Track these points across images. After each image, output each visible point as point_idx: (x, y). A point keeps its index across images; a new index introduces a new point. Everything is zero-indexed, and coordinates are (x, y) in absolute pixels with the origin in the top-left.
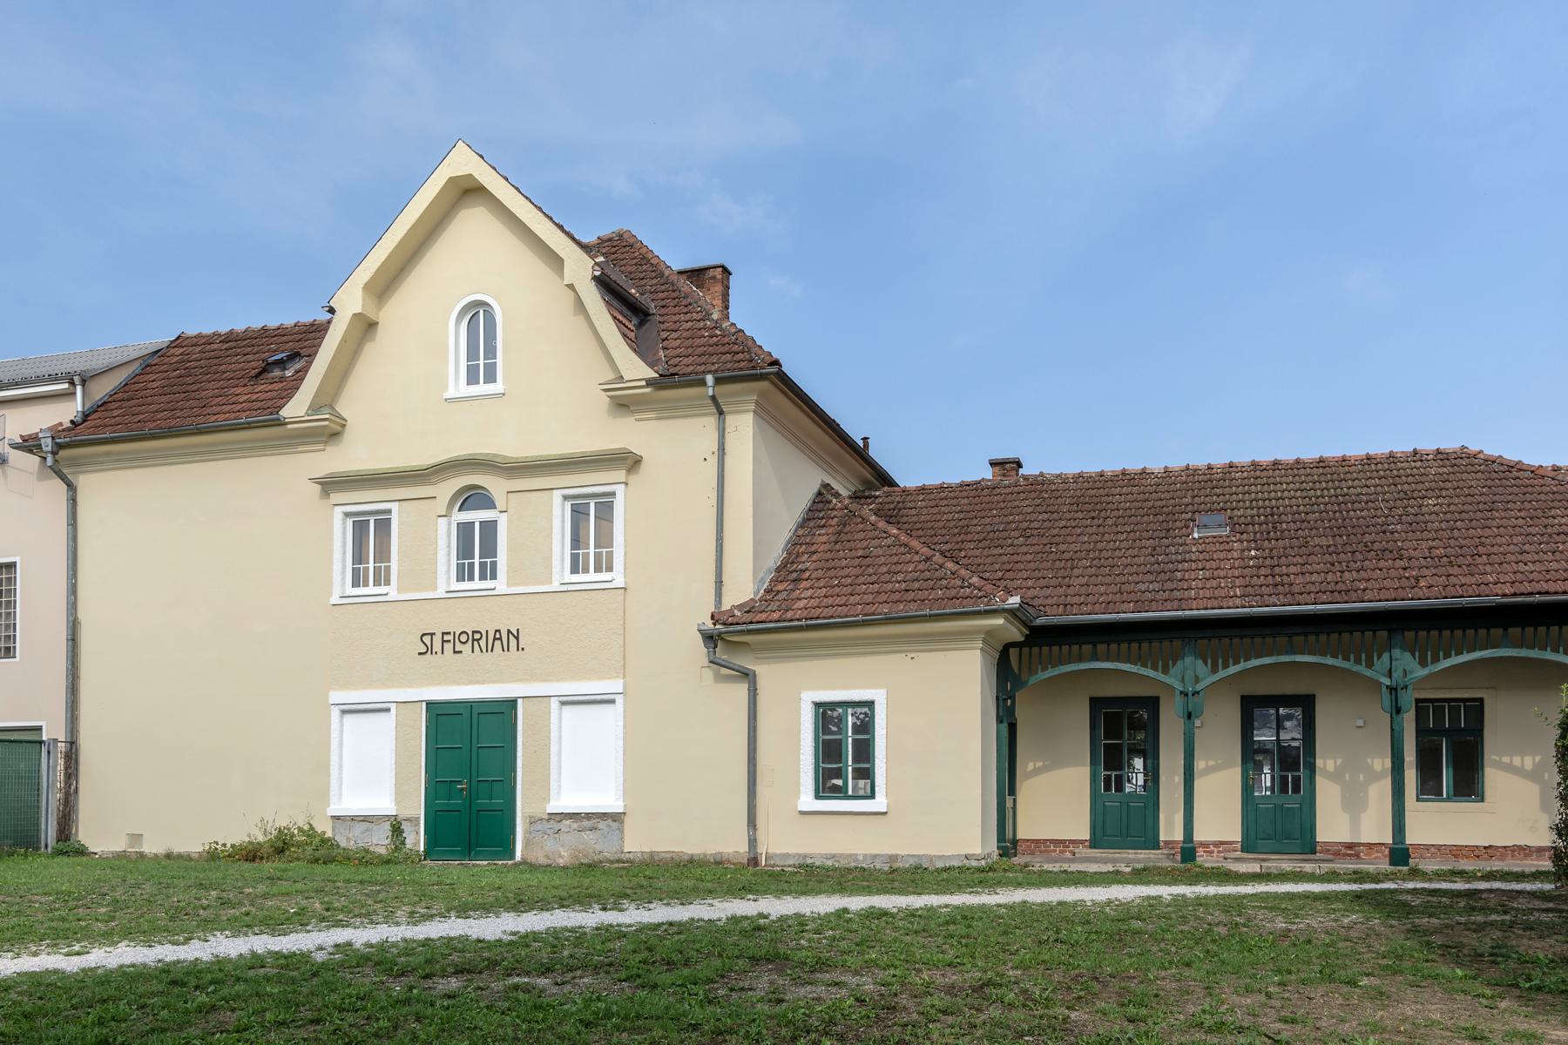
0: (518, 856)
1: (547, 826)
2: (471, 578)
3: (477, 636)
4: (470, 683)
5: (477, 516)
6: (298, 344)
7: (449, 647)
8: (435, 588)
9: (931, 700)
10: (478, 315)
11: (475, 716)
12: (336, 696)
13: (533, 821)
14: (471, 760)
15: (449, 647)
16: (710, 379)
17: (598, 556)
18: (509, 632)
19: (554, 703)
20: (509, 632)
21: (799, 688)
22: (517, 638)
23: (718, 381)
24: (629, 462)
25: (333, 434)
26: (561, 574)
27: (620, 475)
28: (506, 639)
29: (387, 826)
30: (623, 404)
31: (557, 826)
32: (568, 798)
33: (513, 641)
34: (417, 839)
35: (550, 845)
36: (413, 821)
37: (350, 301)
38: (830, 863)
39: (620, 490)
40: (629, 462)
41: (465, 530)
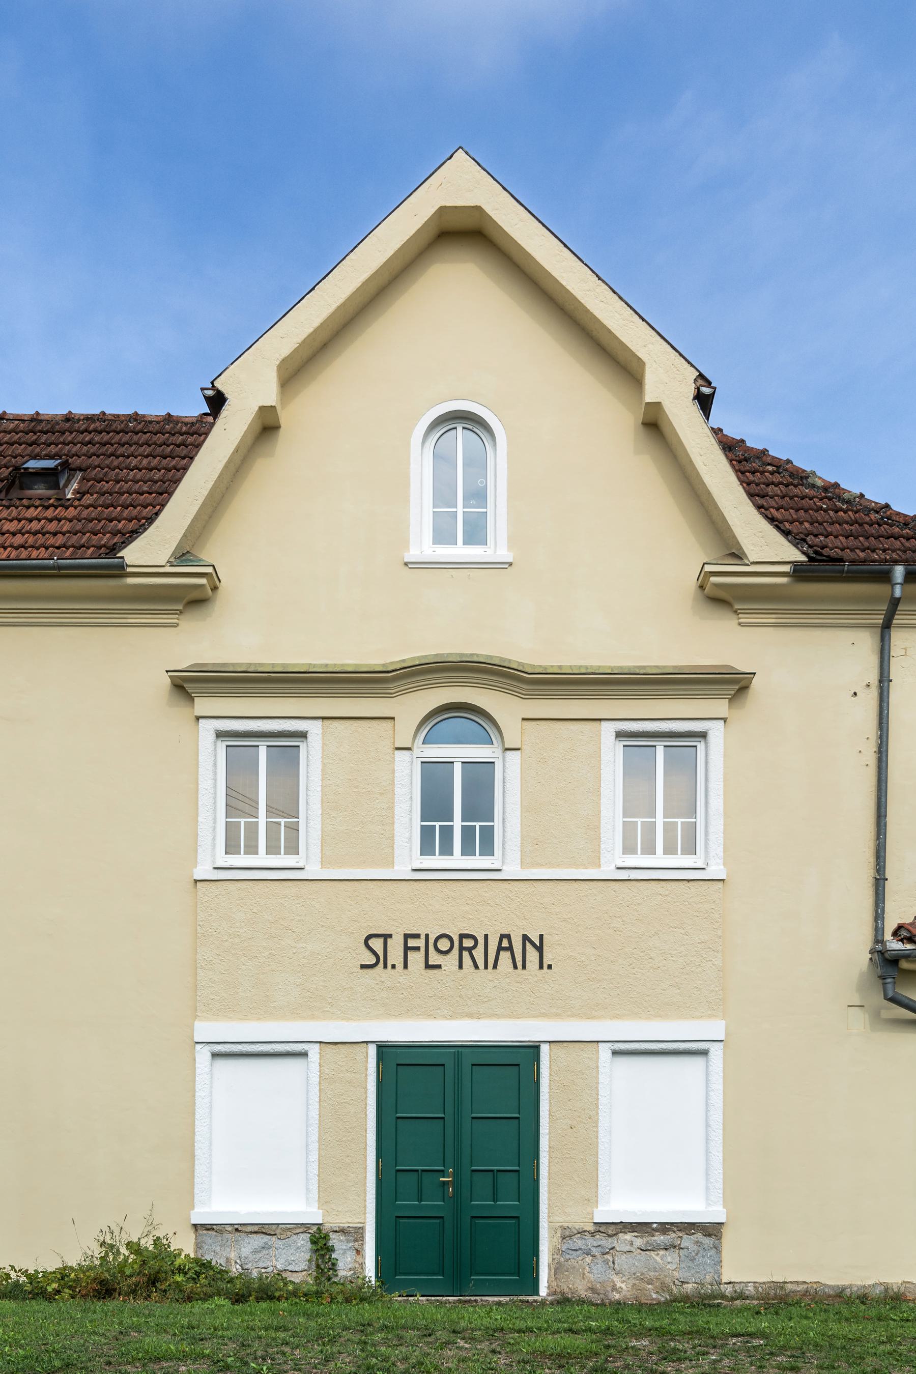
0: (543, 1291)
1: (591, 1242)
2: (447, 850)
3: (468, 943)
5: (458, 753)
6: (174, 443)
7: (416, 958)
8: (389, 862)
11: (467, 1068)
12: (206, 1029)
13: (567, 1235)
15: (416, 958)
16: (899, 572)
17: (272, 829)
18: (525, 938)
19: (605, 1052)
20: (525, 938)
22: (540, 949)
24: (734, 685)
25: (189, 595)
26: (408, 857)
27: (720, 707)
28: (523, 950)
29: (303, 1241)
30: (719, 598)
31: (607, 1243)
34: (362, 1262)
36: (356, 1234)
37: (251, 386)
39: (716, 730)
40: (734, 685)
41: (434, 779)
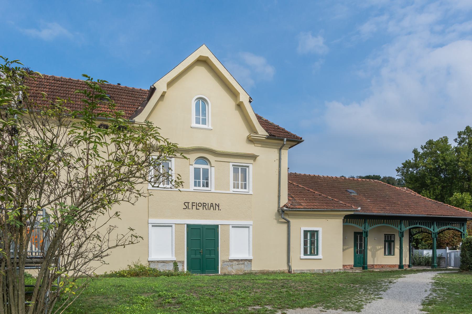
3: (205, 205)
4: (202, 219)
5: (202, 167)
7: (194, 207)
8: (229, 190)
9: (330, 231)
10: (202, 101)
12: (151, 220)
13: (224, 262)
14: (203, 245)
15: (194, 207)
16: (285, 139)
18: (216, 204)
19: (231, 226)
20: (216, 204)
21: (301, 225)
22: (218, 206)
23: (287, 140)
27: (252, 161)
30: (251, 140)
32: (233, 256)
33: (217, 207)
35: (230, 269)
37: (161, 86)
38: (308, 272)
39: (251, 166)
40: (254, 157)
